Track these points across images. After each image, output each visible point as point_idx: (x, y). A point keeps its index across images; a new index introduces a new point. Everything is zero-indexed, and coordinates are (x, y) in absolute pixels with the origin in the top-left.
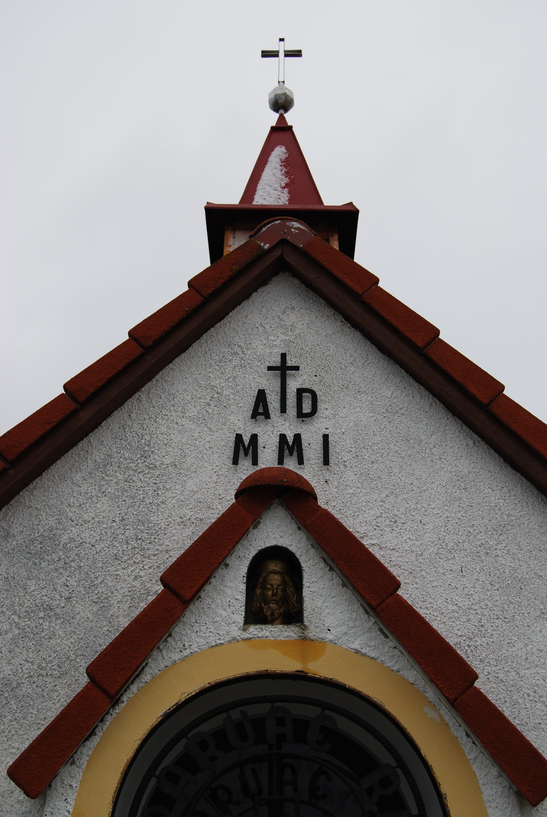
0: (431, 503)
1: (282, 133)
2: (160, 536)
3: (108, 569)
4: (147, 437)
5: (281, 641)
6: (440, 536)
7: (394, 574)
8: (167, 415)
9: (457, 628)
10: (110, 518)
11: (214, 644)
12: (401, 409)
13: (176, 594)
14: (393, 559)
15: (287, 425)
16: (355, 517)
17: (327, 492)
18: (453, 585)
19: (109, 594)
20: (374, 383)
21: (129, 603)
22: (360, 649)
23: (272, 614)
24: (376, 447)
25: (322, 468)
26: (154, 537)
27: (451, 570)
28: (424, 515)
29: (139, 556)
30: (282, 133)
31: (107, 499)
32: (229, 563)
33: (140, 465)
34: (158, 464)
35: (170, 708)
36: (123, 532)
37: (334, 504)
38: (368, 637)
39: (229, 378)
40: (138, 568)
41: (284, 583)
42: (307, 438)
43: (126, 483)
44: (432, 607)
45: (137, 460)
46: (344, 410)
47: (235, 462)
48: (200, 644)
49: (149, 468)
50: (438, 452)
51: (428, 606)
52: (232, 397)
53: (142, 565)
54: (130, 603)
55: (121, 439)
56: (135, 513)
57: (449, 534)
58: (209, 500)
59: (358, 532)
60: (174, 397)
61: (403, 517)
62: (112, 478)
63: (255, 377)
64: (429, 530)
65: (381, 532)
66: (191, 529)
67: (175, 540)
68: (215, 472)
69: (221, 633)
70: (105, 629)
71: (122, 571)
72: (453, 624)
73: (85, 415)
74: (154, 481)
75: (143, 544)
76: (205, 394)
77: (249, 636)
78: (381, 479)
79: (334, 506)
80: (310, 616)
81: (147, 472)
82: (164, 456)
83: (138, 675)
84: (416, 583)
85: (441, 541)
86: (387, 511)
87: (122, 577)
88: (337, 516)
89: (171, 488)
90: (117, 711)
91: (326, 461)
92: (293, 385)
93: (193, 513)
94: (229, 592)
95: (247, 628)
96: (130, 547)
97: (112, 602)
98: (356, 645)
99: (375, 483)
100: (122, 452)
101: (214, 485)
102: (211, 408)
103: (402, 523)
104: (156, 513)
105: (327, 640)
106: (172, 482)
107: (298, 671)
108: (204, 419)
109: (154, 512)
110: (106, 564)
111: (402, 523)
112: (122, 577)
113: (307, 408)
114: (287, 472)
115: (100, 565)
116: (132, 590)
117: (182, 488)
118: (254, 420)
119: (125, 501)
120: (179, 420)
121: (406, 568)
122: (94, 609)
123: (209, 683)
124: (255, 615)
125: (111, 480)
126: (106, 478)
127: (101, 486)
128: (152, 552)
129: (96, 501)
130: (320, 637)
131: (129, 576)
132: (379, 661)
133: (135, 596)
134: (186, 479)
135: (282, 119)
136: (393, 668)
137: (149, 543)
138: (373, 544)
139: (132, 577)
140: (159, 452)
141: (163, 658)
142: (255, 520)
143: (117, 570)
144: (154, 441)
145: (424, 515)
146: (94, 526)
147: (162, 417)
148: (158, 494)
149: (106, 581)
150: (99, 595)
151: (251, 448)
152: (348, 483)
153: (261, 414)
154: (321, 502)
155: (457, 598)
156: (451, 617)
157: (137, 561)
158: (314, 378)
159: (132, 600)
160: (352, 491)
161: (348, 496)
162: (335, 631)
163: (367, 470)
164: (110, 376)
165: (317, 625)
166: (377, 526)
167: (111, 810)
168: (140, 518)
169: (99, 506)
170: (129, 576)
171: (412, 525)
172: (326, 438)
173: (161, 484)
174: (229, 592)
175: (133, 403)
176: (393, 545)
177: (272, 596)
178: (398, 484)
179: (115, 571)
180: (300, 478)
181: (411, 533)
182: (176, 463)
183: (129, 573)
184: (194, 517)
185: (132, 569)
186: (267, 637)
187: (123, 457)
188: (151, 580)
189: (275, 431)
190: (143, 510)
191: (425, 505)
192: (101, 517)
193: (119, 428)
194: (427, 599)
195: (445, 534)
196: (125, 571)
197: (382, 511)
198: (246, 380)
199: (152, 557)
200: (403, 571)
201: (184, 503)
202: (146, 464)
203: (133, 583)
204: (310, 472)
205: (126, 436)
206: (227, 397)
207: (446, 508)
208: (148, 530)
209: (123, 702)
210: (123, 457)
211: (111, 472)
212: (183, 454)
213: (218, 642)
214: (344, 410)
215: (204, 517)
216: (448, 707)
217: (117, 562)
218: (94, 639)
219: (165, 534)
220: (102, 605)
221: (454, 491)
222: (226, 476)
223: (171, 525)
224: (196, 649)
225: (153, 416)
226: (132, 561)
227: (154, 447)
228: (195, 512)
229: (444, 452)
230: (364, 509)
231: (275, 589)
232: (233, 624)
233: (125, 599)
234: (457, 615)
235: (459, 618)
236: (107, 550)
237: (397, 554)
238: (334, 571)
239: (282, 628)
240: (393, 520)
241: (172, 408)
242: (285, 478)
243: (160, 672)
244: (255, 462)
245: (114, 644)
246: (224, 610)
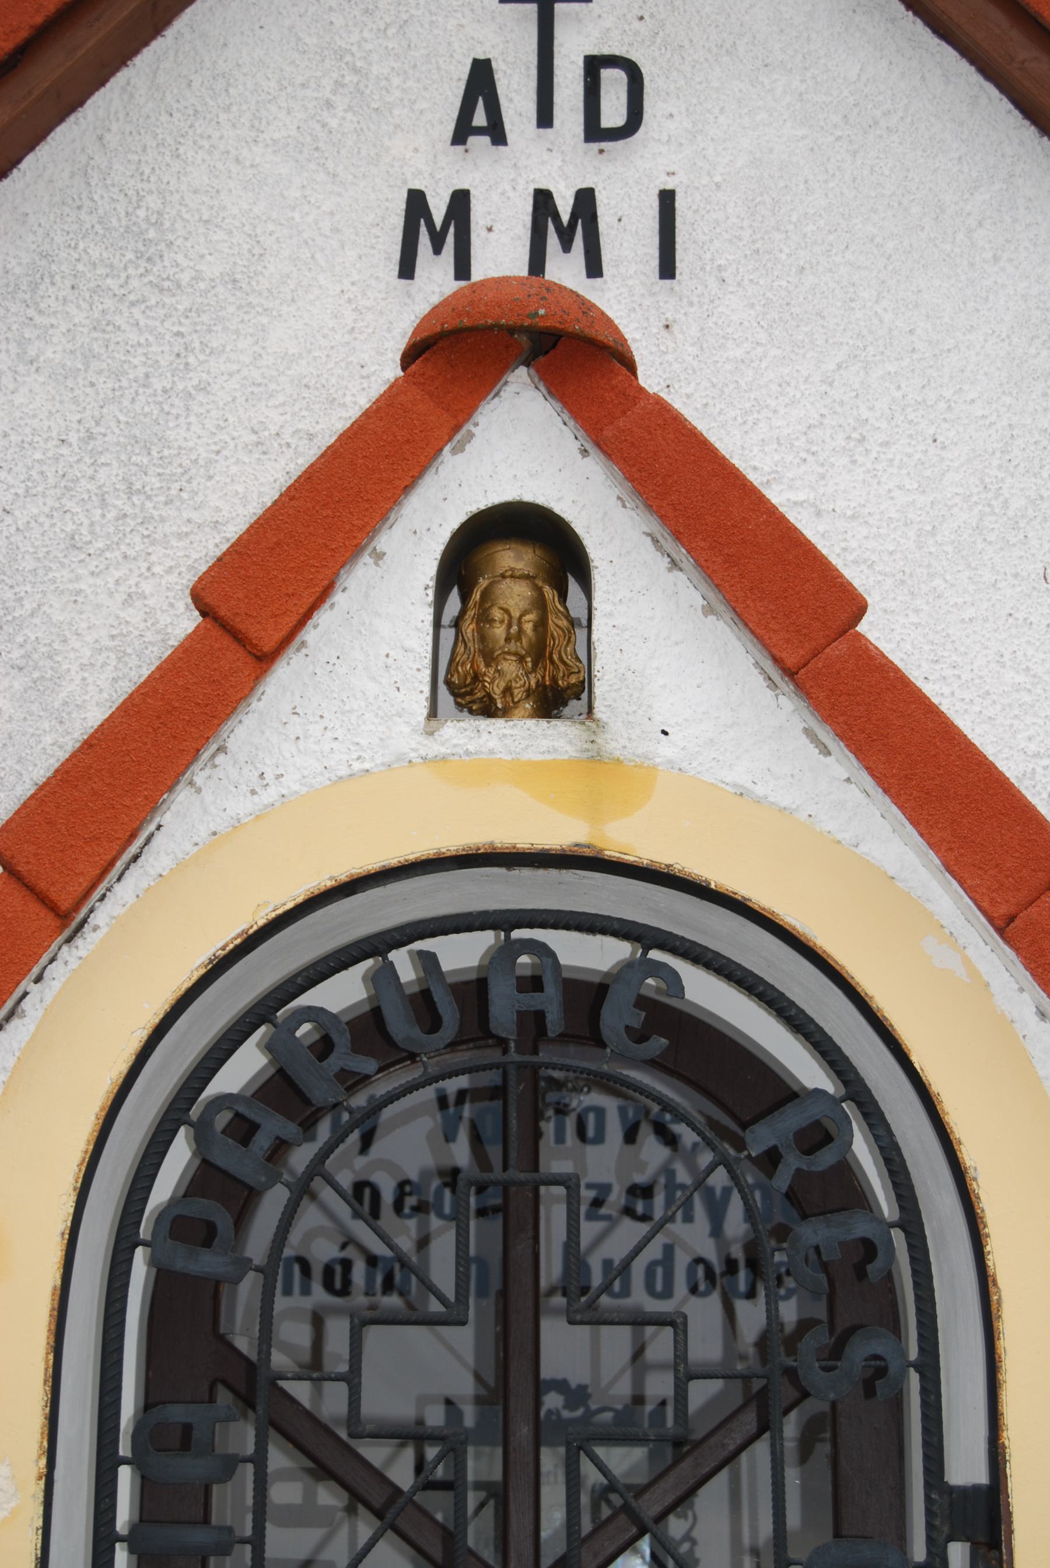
0: (966, 387)
2: (195, 483)
3: (51, 575)
4: (153, 201)
5: (531, 764)
6: (987, 480)
7: (857, 583)
8: (209, 137)
9: (1026, 734)
10: (54, 434)
11: (344, 772)
12: (887, 114)
13: (238, 637)
14: (854, 544)
15: (550, 159)
16: (746, 428)
17: (670, 357)
18: (1020, 616)
19: (56, 646)
20: (809, 39)
21: (110, 668)
22: (749, 785)
23: (508, 690)
24: (811, 227)
25: (656, 289)
26: (177, 486)
27: (1016, 576)
28: (945, 420)
29: (138, 539)
31: (41, 379)
32: (384, 550)
33: (134, 283)
34: (185, 277)
35: (226, 945)
36: (90, 472)
37: (689, 390)
39: (388, 26)
40: (137, 572)
42: (613, 202)
43: (95, 335)
44: (959, 677)
45: (125, 268)
46: (722, 119)
47: (407, 269)
48: (306, 773)
49: (162, 290)
50: (990, 241)
51: (949, 672)
52: (396, 81)
53: (146, 565)
54: (116, 669)
55: (79, 208)
56: (122, 418)
57: (1012, 476)
58: (333, 380)
59: (755, 468)
60: (229, 85)
61: (884, 425)
62: (53, 321)
63: (464, 22)
64: (956, 464)
65: (821, 470)
66: (282, 461)
67: (237, 493)
68: (349, 301)
69: (364, 742)
70: (48, 739)
71: (91, 580)
72: (1016, 722)
74: (175, 329)
75: (149, 505)
76: (319, 74)
77: (443, 750)
78: (823, 318)
79: (688, 396)
80: (613, 694)
81: (153, 302)
82: (202, 256)
83: (136, 858)
84: (917, 611)
85: (990, 495)
86: (839, 410)
87: (92, 597)
88: (701, 425)
89: (224, 346)
90: (82, 953)
91: (667, 269)
93: (288, 417)
94: (385, 611)
95: (438, 729)
96: (111, 515)
97: (65, 667)
98: (739, 775)
99: (806, 329)
100: (81, 246)
101: (347, 338)
102: (334, 116)
103: (881, 445)
104: (182, 420)
105: (658, 760)
106: (225, 329)
107: (577, 845)
108: (317, 149)
109: (177, 417)
110: (47, 563)
111: (881, 445)
112: (92, 597)
114: (548, 289)
115: (29, 564)
116: (121, 634)
117: (256, 348)
118: (460, 148)
119: (92, 385)
120: (245, 152)
121: (888, 570)
122: (17, 685)
123: (331, 879)
124: (466, 689)
125: (52, 326)
126: (39, 320)
127: (23, 343)
128: (175, 528)
129: (11, 386)
130: (640, 751)
131: (111, 594)
132: (803, 816)
133: (129, 650)
134: (264, 320)
136: (839, 837)
137: (166, 503)
138: (796, 503)
139: (120, 597)
140: (189, 244)
141: (205, 811)
142: (457, 428)
143: (78, 578)
144: (174, 212)
145: (945, 420)
146: (9, 457)
147: (195, 143)
148: (187, 364)
149: (45, 608)
150: (29, 647)
151: (452, 230)
152: (729, 330)
153: (479, 131)
154: (650, 378)
155: (1030, 652)
156: (1010, 705)
157: (131, 553)
158: (637, 24)
159: (119, 659)
160: (739, 353)
161: (728, 367)
162: (690, 743)
163: (783, 294)
164: (39, 20)
165: (631, 718)
166: (808, 451)
167: (72, 1210)
168: (136, 431)
169: (19, 399)
170: (111, 594)
171: (909, 450)
172: (667, 199)
173: (195, 336)
174: (385, 611)
175: (111, 100)
176: (853, 504)
177: (508, 639)
178: (871, 332)
179: (70, 581)
180: (586, 307)
181: (904, 472)
182: (238, 276)
183: (111, 585)
184: (292, 429)
185: (117, 574)
186: (491, 752)
187: (85, 257)
188: (172, 605)
189: (521, 182)
190: (147, 409)
191: (948, 393)
192: (28, 430)
193: (72, 175)
194: (946, 654)
195: (1000, 475)
196: (99, 581)
197: (823, 411)
198: (436, 32)
199: (174, 543)
200: (880, 578)
201: (260, 389)
202: (151, 278)
203: (122, 615)
204: (623, 296)
205: (92, 199)
206: (383, 83)
207: (1008, 400)
208: (160, 466)
209: (96, 928)
210: (85, 257)
211: (51, 301)
212: (257, 251)
213: (357, 766)
214: (722, 119)
215: (319, 427)
216: (988, 939)
217: (77, 556)
218: (18, 767)
219: (210, 478)
220: (36, 675)
221: (1033, 351)
222: (381, 313)
223: (225, 453)
224: (296, 787)
225: (170, 140)
226: (117, 553)
227: (173, 230)
228: (294, 414)
229: (1007, 241)
230: (773, 403)
231: (515, 622)
232: (397, 719)
233: (101, 659)
234: (1027, 698)
235: (1032, 706)
236: (47, 523)
237: (864, 531)
238: (681, 570)
239: (533, 728)
240: (855, 435)
241: (223, 117)
242: (544, 307)
243: (196, 849)
244: (462, 269)
245: (67, 772)
246: (373, 679)
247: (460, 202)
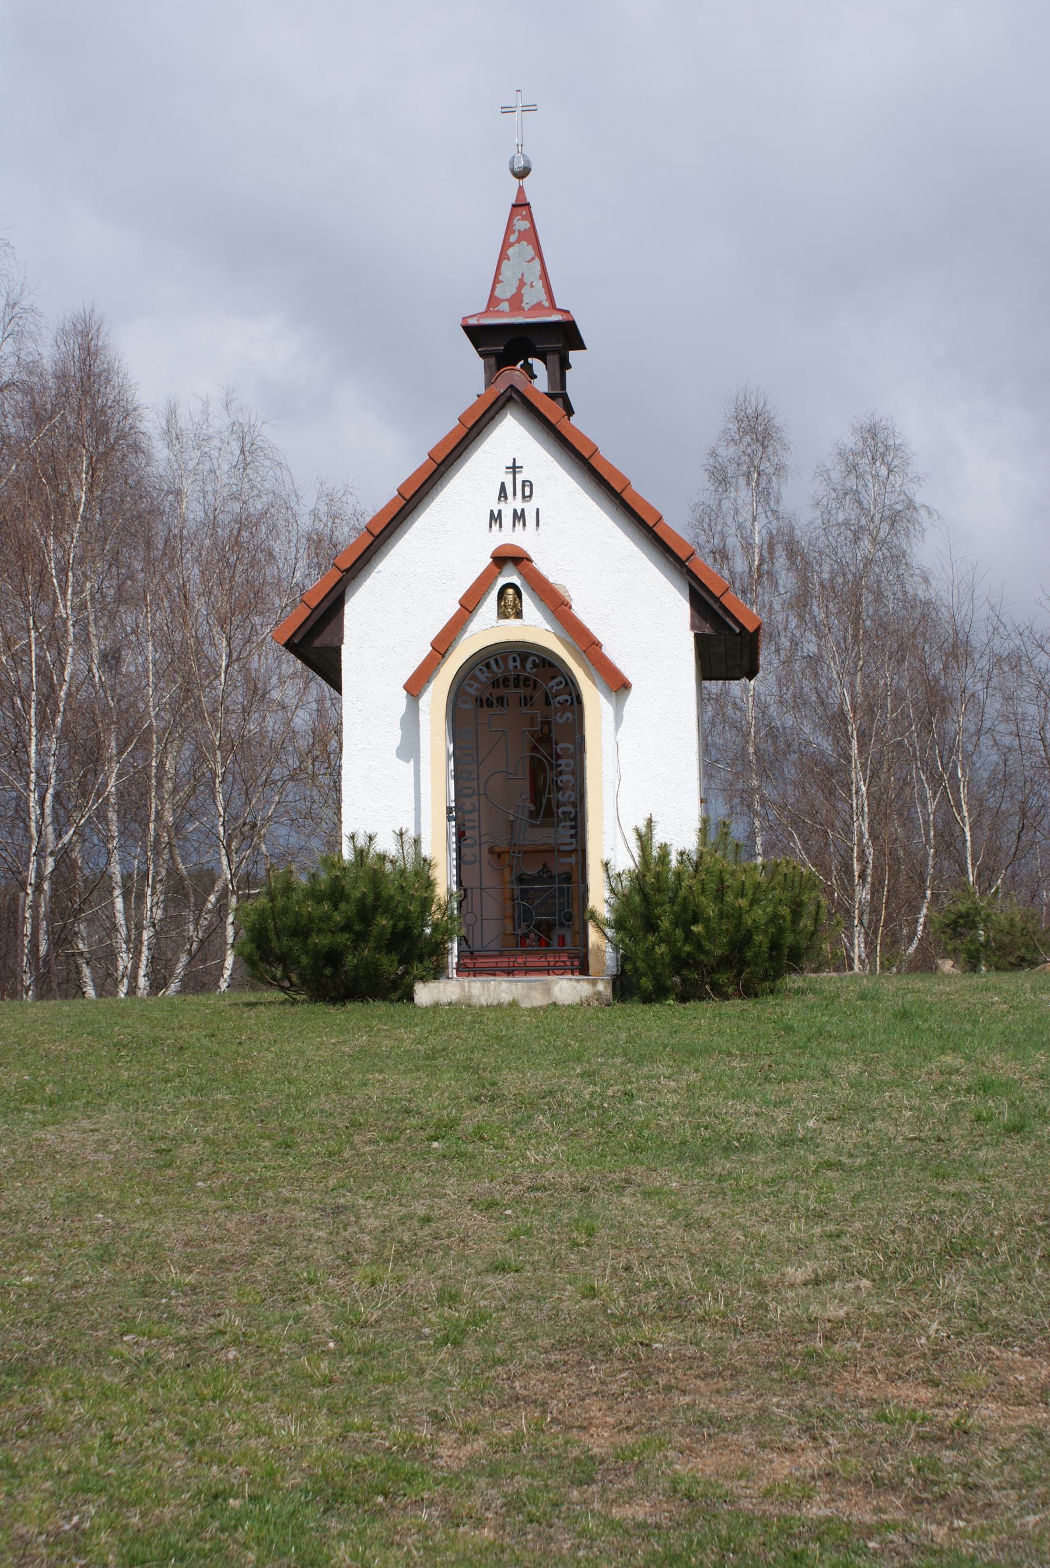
1: (521, 206)
30: (521, 206)
38: (8, 996)
41: (515, 599)
73: (442, 468)
91: (538, 525)
92: (520, 478)
94: (491, 602)
113: (527, 493)
124: (502, 614)
135: (521, 190)
162: (534, 627)
174: (491, 602)
247: (500, 511)
